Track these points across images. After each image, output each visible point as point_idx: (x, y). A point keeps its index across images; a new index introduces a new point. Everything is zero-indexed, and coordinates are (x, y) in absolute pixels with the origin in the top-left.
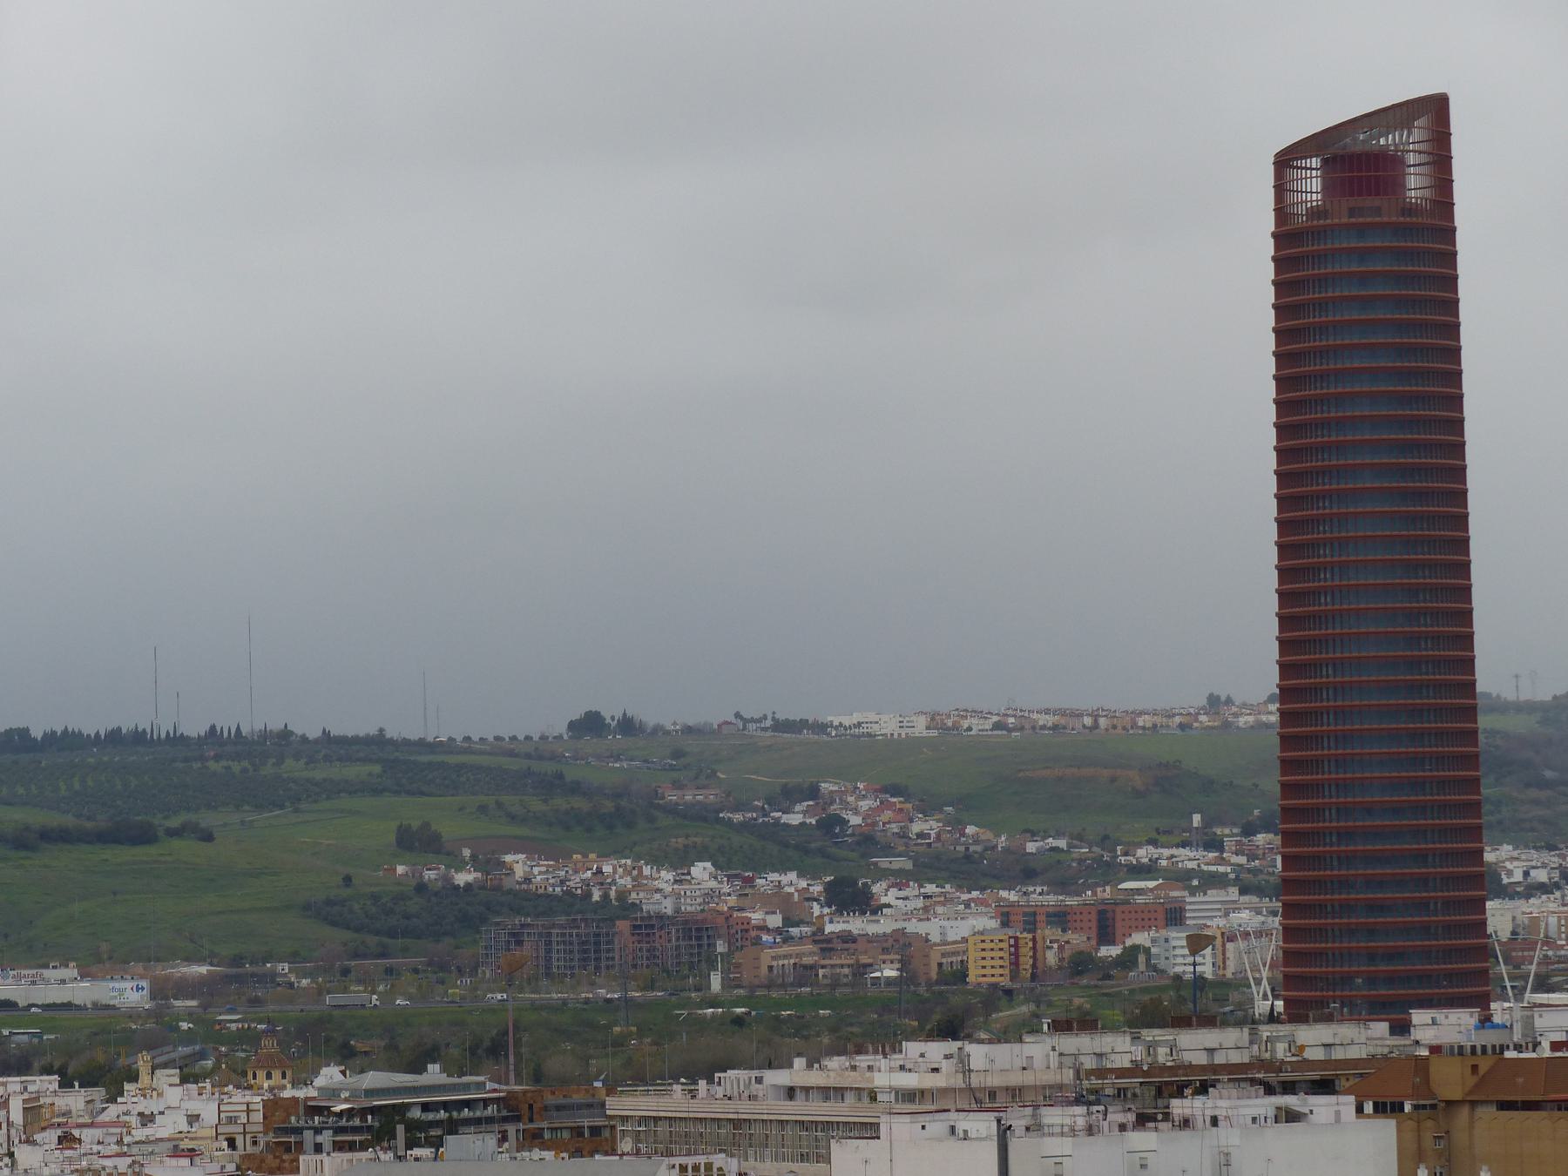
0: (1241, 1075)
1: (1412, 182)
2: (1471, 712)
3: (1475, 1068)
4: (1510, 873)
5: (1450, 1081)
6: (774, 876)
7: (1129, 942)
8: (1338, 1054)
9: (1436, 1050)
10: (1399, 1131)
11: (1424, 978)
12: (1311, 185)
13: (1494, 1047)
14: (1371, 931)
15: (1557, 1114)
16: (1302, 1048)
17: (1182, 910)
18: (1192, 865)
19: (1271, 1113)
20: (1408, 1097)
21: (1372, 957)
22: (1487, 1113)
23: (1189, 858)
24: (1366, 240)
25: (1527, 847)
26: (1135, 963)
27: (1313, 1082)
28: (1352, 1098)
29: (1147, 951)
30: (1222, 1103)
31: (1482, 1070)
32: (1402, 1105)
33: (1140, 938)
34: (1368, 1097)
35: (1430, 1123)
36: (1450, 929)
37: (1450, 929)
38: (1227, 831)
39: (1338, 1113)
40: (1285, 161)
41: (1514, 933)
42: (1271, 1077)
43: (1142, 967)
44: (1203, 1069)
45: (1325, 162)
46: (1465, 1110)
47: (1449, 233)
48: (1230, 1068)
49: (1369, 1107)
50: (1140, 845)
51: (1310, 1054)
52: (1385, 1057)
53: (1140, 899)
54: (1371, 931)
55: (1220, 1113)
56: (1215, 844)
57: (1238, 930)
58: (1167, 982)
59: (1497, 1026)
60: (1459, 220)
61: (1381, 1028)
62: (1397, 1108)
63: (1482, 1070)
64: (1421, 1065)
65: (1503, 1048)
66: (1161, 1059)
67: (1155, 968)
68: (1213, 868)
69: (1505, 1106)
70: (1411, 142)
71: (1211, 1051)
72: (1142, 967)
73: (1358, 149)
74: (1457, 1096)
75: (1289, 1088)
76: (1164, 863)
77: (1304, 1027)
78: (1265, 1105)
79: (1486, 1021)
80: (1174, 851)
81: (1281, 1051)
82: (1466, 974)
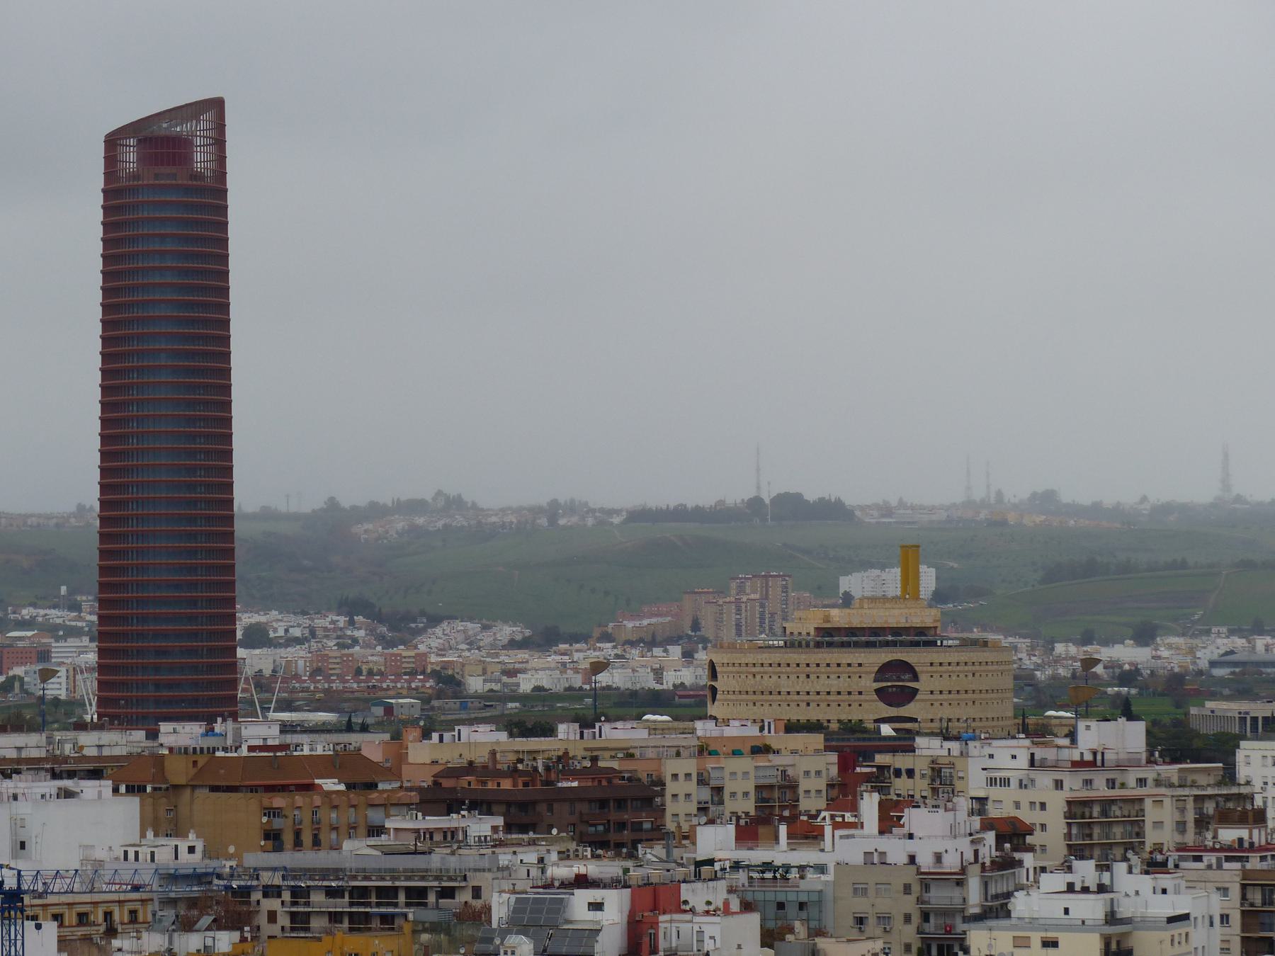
0: (34, 765)
1: (198, 157)
2: (230, 519)
3: (195, 763)
4: (275, 630)
5: (179, 772)
6: (31, 609)
7: (11, 673)
8: (106, 752)
9: (171, 749)
10: (142, 805)
11: (170, 702)
12: (130, 157)
13: (202, 749)
14: (157, 669)
15: (250, 795)
16: (82, 748)
17: (49, 652)
18: (59, 621)
19: (54, 792)
20: (149, 782)
21: (158, 685)
22: (202, 793)
23: (57, 616)
24: (166, 211)
25: (288, 612)
26: (12, 688)
27: (89, 771)
28: (110, 782)
29: (21, 679)
30: (21, 785)
31: (200, 764)
32: (145, 788)
33: (18, 671)
34: (122, 781)
35: (164, 800)
36: (211, 668)
37: (211, 668)
38: (84, 598)
39: (100, 792)
40: (113, 142)
41: (274, 671)
42: (57, 768)
43: (17, 690)
44: (12, 760)
45: (139, 141)
46: (188, 791)
47: (224, 192)
48: (30, 761)
49: (123, 789)
50: (24, 606)
51: (86, 752)
52: (139, 755)
53: (20, 644)
54: (157, 669)
55: (18, 791)
56: (76, 607)
57: (74, 665)
58: (34, 701)
59: (217, 735)
60: (230, 185)
61: (139, 735)
62: (142, 789)
63: (200, 764)
64: (158, 760)
65: (214, 750)
66: (67, 752)
67: (27, 692)
68: (73, 623)
69: (215, 789)
70: (200, 130)
71: (19, 749)
72: (17, 690)
73: (163, 133)
74: (183, 782)
75: (71, 775)
76: (40, 619)
77: (83, 733)
78: (52, 786)
79: (210, 731)
80: (48, 611)
81: (68, 749)
82: (215, 695)
